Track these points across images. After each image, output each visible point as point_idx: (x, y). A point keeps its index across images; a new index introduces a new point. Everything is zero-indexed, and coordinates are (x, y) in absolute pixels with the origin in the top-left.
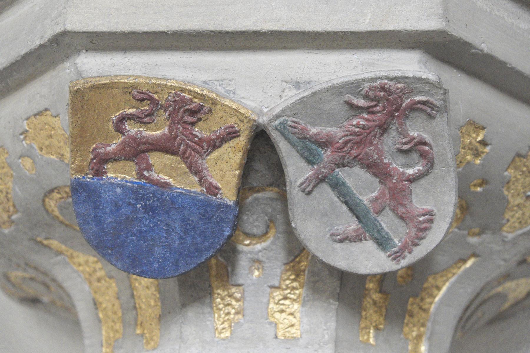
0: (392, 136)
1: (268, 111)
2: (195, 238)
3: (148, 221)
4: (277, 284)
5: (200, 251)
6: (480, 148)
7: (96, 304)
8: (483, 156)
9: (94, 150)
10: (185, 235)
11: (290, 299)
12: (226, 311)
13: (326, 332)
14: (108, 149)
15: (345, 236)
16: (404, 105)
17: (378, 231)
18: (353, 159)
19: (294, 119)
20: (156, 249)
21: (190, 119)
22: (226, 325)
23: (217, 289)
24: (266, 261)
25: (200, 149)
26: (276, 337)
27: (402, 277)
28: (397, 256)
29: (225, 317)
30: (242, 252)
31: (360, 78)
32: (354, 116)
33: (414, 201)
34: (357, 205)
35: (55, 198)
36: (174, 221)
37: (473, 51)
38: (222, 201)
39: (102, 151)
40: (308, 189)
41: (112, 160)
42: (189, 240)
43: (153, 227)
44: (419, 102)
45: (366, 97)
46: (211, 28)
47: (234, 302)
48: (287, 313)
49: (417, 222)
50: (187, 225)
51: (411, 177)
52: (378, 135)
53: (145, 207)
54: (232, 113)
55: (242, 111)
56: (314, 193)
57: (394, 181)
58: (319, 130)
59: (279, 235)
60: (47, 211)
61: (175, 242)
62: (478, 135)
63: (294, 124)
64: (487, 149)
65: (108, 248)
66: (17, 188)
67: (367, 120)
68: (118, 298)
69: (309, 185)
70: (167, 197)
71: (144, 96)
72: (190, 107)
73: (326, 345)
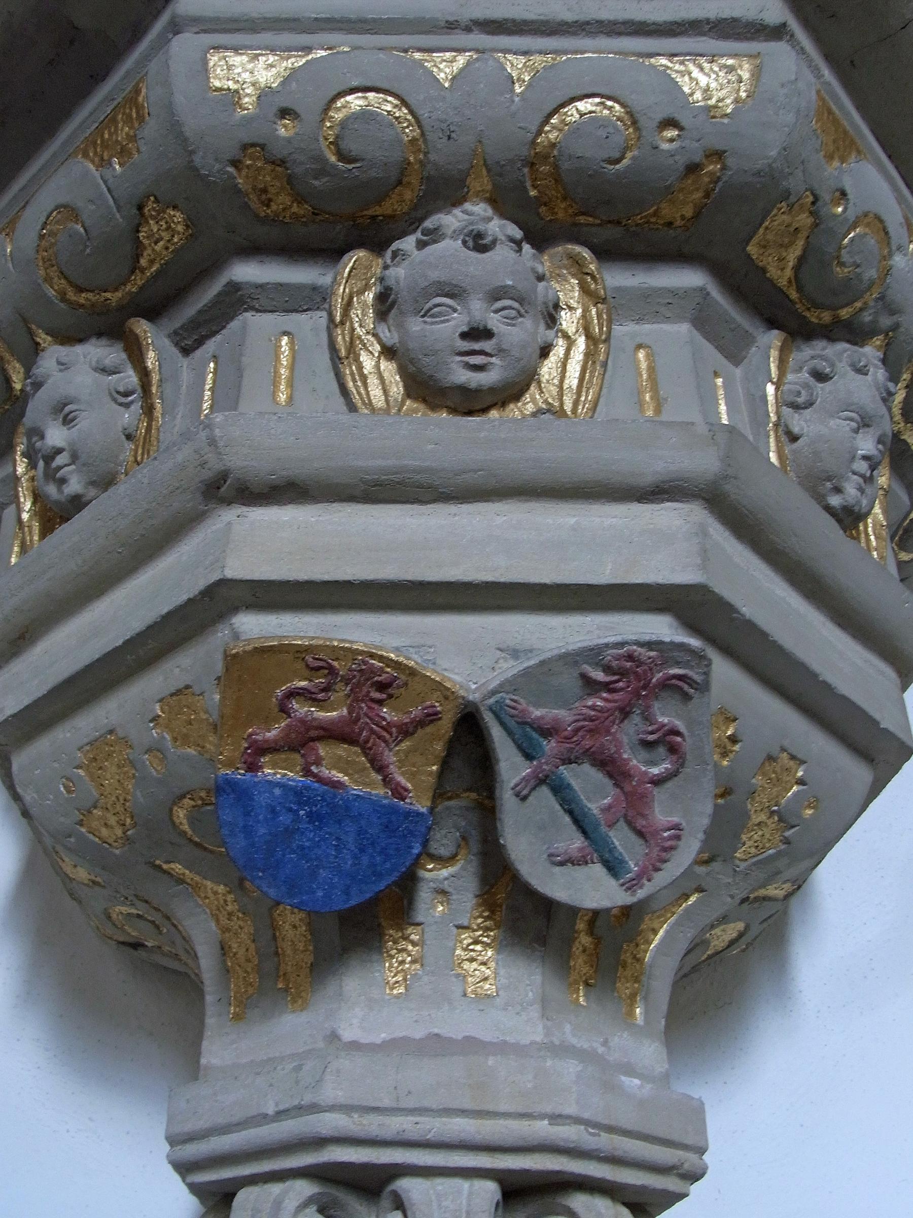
0: (634, 722)
1: (476, 688)
2: (374, 857)
3: (312, 834)
4: (466, 924)
5: (379, 876)
6: (729, 746)
7: (224, 948)
8: (731, 756)
9: (250, 735)
10: (360, 853)
11: (482, 943)
12: (400, 959)
13: (529, 988)
14: (268, 734)
15: (567, 857)
16: (654, 680)
17: (610, 851)
18: (584, 752)
19: (514, 697)
20: (321, 871)
21: (377, 695)
22: (399, 978)
23: (388, 929)
24: (453, 892)
25: (387, 736)
26: (465, 995)
27: (615, 916)
28: (631, 886)
29: (397, 967)
30: (423, 879)
31: (603, 642)
32: (589, 695)
33: (657, 810)
34: (585, 815)
35: (185, 806)
36: (346, 833)
37: (735, 615)
38: (412, 807)
39: (259, 738)
40: (525, 792)
41: (271, 750)
42: (365, 860)
43: (319, 841)
44: (675, 677)
45: (607, 669)
46: (410, 578)
47: (410, 948)
48: (479, 962)
49: (660, 839)
50: (364, 838)
51: (655, 778)
52: (617, 722)
53: (309, 815)
54: (434, 687)
55: (448, 685)
56: (530, 798)
57: (634, 783)
58: (544, 713)
59: (472, 857)
60: (173, 823)
61: (346, 863)
62: (727, 728)
63: (513, 704)
64: (737, 748)
65: (259, 870)
66: (139, 794)
67: (606, 700)
68: (254, 941)
69: (526, 786)
70: (341, 802)
71: (321, 664)
72: (380, 679)
73: (531, 1006)
